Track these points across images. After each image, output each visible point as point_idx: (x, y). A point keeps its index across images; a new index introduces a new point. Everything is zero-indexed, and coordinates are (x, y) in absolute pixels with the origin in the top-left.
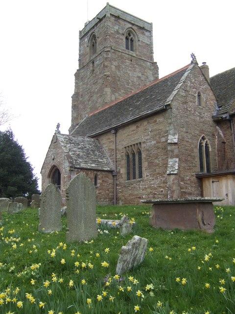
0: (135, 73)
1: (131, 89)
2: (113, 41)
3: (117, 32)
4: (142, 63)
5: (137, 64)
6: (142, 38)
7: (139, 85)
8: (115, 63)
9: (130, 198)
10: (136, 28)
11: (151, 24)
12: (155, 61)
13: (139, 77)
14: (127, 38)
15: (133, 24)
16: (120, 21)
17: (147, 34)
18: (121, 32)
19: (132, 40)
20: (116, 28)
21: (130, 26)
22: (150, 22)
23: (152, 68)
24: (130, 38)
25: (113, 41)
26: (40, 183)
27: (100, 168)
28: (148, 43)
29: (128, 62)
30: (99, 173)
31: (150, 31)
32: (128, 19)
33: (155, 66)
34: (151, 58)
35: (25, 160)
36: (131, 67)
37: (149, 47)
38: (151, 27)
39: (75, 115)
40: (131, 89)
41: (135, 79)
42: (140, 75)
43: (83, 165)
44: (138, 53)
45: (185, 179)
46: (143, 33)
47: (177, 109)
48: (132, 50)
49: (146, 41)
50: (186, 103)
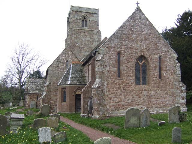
0: (86, 39)
1: (84, 47)
2: (82, 20)
3: (77, 19)
4: (91, 32)
5: (88, 34)
6: (90, 18)
7: (89, 44)
8: (74, 36)
9: (152, 136)
10: (88, 14)
11: (98, 10)
12: (99, 30)
13: (89, 40)
14: (83, 20)
15: (86, 13)
16: (78, 13)
17: (95, 15)
18: (79, 19)
19: (86, 21)
20: (76, 17)
21: (85, 14)
22: (97, 8)
23: (98, 33)
24: (85, 20)
25: (82, 20)
26: (164, 122)
27: (39, 93)
28: (96, 20)
29: (82, 34)
30: (39, 95)
31: (97, 14)
32: (83, 10)
33: (99, 32)
34: (97, 28)
35: (7, 87)
36: (84, 36)
37: (96, 23)
38: (98, 11)
39: (56, 63)
40: (84, 47)
41: (86, 42)
42: (89, 39)
43: (31, 92)
44: (89, 27)
45: (54, 99)
46: (93, 16)
47: (52, 71)
48: (86, 26)
49: (94, 19)
50: (57, 67)
